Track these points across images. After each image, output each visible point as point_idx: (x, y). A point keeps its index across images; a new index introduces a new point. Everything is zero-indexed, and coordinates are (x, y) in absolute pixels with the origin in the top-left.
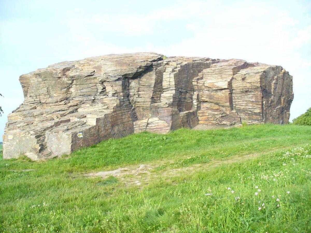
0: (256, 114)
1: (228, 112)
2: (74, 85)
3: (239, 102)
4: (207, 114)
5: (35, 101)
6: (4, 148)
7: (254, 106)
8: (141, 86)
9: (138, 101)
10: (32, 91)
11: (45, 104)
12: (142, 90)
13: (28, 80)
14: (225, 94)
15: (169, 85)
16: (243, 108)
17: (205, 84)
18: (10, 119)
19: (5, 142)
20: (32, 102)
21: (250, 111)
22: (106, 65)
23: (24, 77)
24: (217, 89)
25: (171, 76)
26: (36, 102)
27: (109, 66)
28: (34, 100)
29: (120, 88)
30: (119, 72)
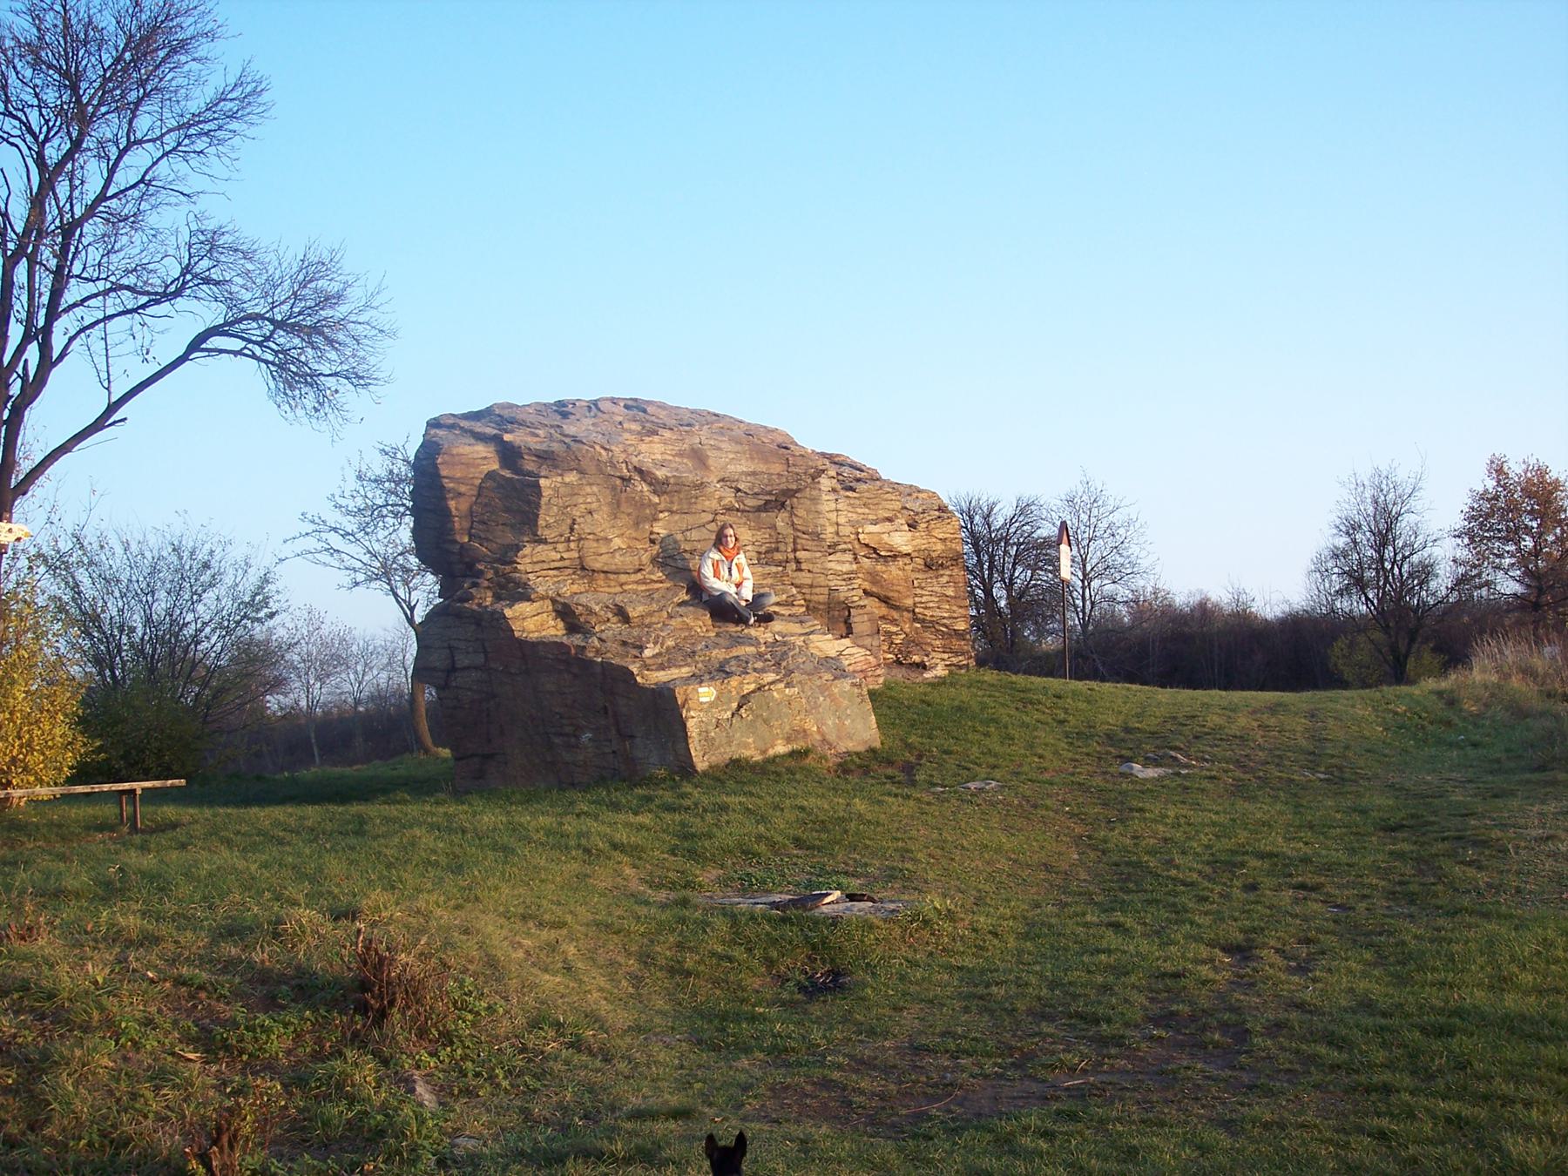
0: (959, 635)
2: (666, 514)
3: (922, 596)
5: (562, 559)
6: (694, 734)
7: (954, 612)
8: (799, 534)
11: (602, 575)
13: (472, 470)
15: (837, 534)
16: (932, 616)
17: (861, 537)
19: (692, 713)
20: (553, 565)
22: (719, 449)
23: (458, 455)
24: (889, 554)
25: (839, 507)
26: (567, 563)
27: (731, 456)
28: (559, 557)
30: (766, 481)
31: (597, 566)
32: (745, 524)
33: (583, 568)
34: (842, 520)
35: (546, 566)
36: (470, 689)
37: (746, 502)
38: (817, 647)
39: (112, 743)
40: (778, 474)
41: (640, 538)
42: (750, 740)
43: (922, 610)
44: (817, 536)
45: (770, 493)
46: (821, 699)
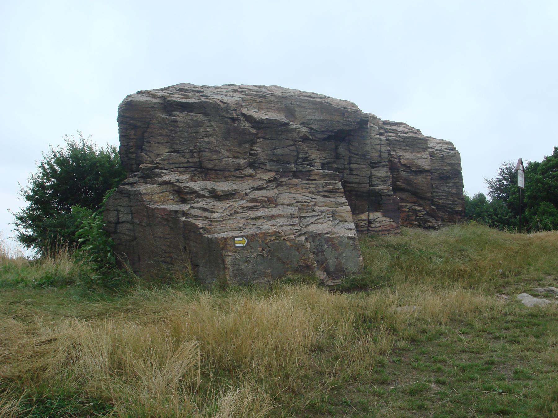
1: (428, 207)
2: (262, 140)
3: (437, 193)
4: (407, 210)
5: (188, 162)
6: (229, 266)
7: (456, 201)
8: (353, 155)
9: (350, 180)
10: (179, 140)
12: (354, 162)
14: (426, 178)
15: (380, 156)
17: (402, 161)
18: (149, 199)
19: (229, 253)
21: (450, 208)
22: (303, 107)
24: (417, 170)
26: (191, 165)
27: (309, 111)
28: (186, 160)
29: (331, 154)
31: (210, 166)
32: (315, 147)
33: (201, 167)
34: (383, 149)
35: (177, 166)
36: (125, 234)
37: (316, 135)
38: (340, 216)
39: (306, 239)
40: (338, 121)
41: (242, 152)
42: (269, 271)
43: (437, 200)
44: (364, 156)
45: (332, 131)
46: (326, 246)
